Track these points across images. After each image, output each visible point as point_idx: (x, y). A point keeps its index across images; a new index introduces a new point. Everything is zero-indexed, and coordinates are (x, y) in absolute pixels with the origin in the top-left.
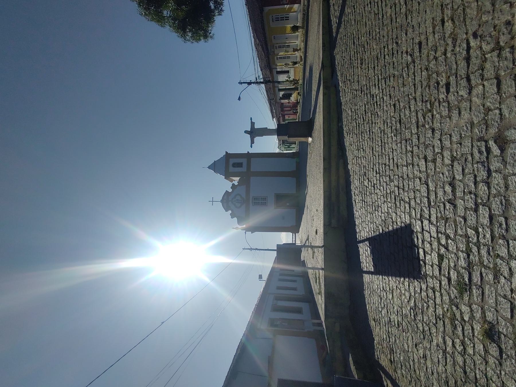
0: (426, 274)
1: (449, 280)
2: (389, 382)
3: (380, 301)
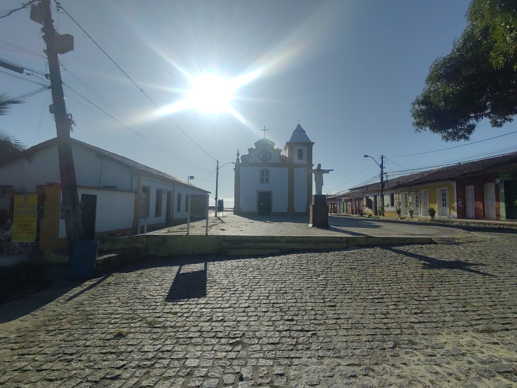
0: (166, 305)
1: (159, 317)
2: (95, 282)
3: (155, 277)
